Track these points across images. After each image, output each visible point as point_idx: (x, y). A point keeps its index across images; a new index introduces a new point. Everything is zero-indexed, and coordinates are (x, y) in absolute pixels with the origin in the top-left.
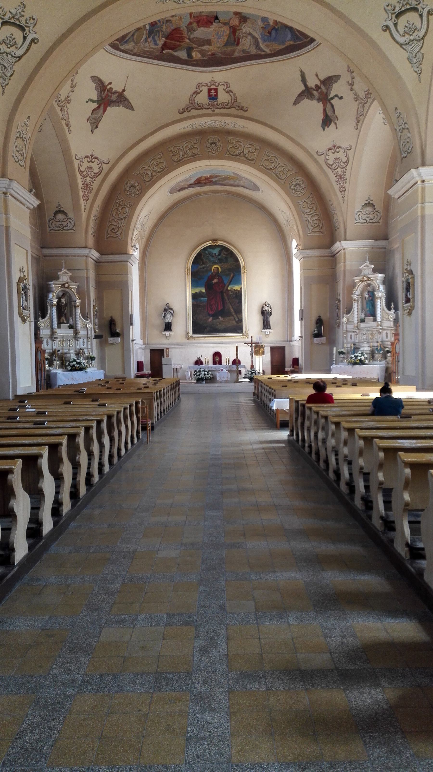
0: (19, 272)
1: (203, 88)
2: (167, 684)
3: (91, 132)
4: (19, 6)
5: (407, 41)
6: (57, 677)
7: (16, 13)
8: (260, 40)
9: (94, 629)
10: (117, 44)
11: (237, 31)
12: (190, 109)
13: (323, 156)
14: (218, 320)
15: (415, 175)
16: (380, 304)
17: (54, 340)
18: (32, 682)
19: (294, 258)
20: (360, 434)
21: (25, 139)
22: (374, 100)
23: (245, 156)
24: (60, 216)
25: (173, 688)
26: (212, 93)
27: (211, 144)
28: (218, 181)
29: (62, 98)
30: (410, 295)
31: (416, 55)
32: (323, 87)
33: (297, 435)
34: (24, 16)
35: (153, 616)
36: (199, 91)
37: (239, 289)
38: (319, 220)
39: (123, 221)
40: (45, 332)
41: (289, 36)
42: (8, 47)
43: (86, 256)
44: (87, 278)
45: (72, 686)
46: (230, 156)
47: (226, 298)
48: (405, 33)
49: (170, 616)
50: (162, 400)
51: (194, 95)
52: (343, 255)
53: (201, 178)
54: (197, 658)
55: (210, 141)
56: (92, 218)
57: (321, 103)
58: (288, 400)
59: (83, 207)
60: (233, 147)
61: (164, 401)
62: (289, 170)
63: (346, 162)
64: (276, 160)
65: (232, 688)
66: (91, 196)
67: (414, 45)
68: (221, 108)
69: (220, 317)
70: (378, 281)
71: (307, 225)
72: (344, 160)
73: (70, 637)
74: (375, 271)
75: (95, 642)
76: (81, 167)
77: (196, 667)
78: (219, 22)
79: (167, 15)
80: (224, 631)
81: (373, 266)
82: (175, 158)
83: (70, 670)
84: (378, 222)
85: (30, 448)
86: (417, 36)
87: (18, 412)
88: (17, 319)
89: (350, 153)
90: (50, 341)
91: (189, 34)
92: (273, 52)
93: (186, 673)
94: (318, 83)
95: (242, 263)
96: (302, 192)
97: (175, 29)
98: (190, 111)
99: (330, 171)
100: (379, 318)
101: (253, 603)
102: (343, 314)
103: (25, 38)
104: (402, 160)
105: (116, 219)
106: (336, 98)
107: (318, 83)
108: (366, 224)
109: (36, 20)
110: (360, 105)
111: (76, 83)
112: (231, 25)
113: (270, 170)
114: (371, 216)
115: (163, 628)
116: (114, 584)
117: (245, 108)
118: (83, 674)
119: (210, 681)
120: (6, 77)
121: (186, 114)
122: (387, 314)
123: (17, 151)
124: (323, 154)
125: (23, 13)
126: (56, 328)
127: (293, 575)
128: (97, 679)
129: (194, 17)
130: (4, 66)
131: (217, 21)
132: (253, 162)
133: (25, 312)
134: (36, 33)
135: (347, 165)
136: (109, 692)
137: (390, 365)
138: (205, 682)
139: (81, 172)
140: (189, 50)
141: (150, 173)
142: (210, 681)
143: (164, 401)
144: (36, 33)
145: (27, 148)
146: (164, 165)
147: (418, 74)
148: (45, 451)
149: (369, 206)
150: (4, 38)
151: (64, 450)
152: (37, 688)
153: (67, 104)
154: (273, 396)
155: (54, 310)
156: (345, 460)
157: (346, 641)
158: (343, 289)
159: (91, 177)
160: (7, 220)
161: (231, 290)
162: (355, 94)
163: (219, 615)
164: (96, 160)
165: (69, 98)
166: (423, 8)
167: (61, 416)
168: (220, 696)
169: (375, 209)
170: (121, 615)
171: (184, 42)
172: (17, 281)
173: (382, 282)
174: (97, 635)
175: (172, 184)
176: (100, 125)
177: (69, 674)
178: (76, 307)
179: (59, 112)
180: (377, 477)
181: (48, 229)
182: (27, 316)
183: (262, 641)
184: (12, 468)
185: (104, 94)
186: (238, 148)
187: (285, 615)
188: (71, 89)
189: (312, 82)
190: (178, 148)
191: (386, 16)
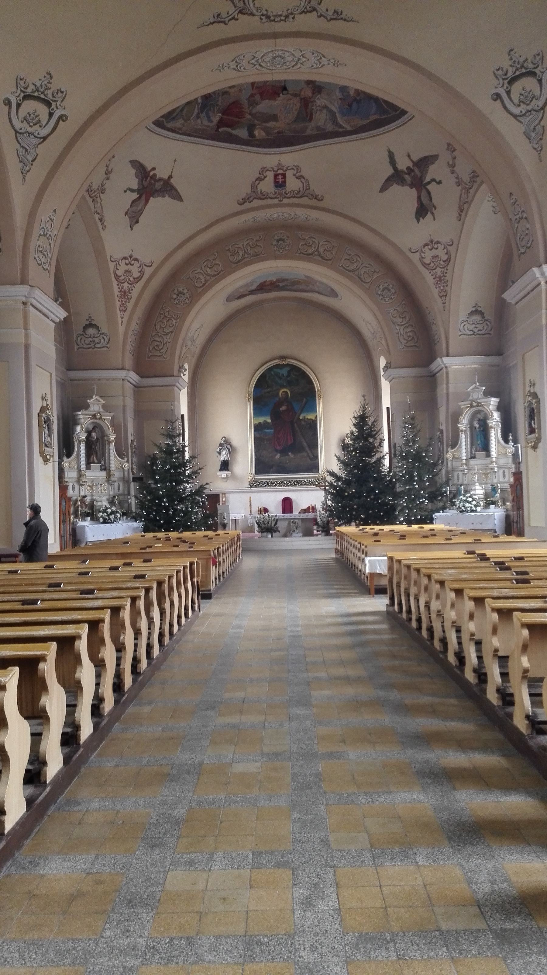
0: (41, 400)
1: (268, 173)
2: (262, 952)
3: (130, 229)
4: (45, 77)
5: (524, 112)
6: (112, 942)
7: (42, 85)
8: (337, 114)
9: (156, 873)
10: (163, 121)
11: (310, 104)
12: (252, 199)
13: (418, 253)
14: (287, 457)
15: (538, 275)
16: (495, 435)
17: (81, 485)
18: (79, 948)
19: (383, 379)
20: (493, 605)
21: (50, 237)
22: (482, 183)
23: (320, 255)
24: (91, 331)
25: (270, 957)
26: (279, 179)
27: (278, 241)
28: (287, 286)
29: (95, 187)
30: (534, 424)
31: (534, 129)
32: (417, 171)
33: (400, 604)
34: (50, 89)
35: (234, 854)
36: (263, 177)
37: (314, 418)
38: (415, 332)
39: (168, 337)
40: (71, 475)
41: (374, 110)
42: (30, 126)
43: (123, 380)
44: (124, 406)
45: (134, 954)
46: (301, 255)
47: (297, 429)
48: (521, 101)
49: (256, 854)
50: (221, 559)
51: (257, 182)
52: (445, 373)
53: (265, 282)
54: (298, 913)
55: (276, 238)
56: (130, 333)
57: (414, 189)
58: (386, 558)
59: (120, 319)
60: (305, 244)
61: (224, 561)
62: (375, 272)
63: (447, 260)
64: (359, 259)
65: (351, 957)
66: (130, 306)
67: (532, 116)
68: (290, 198)
69: (290, 453)
70: (491, 407)
71: (399, 338)
72: (445, 257)
73: (126, 884)
74: (488, 394)
75: (159, 891)
76: (117, 271)
77: (299, 927)
78: (288, 93)
79: (224, 86)
80: (331, 875)
81: (484, 388)
82: (235, 258)
83: (128, 931)
84: (490, 334)
85: (64, 626)
86: (536, 106)
87: (19, 574)
88: (38, 459)
89: (452, 249)
90: (76, 486)
91: (251, 108)
92: (354, 129)
93: (285, 935)
94: (411, 165)
95: (317, 385)
96: (392, 298)
97: (234, 103)
98: (252, 201)
99: (427, 272)
100: (494, 453)
101: (366, 836)
102: (447, 447)
103: (51, 115)
104: (519, 256)
105: (160, 334)
106: (433, 183)
107: (411, 165)
108: (473, 336)
109: (65, 93)
110: (464, 191)
111: (112, 169)
112: (303, 97)
113: (350, 271)
114: (480, 327)
115: (249, 870)
116: (178, 810)
117: (319, 197)
118: (148, 937)
119: (320, 947)
120: (27, 162)
121: (247, 205)
122: (504, 447)
123: (41, 251)
124: (417, 251)
125: (49, 85)
126: (84, 469)
127: (415, 796)
128: (166, 944)
129: (257, 87)
130: (25, 149)
131: (284, 92)
132: (330, 262)
133: (48, 450)
134: (64, 109)
135: (448, 264)
136: (184, 963)
137: (511, 513)
138: (313, 949)
139: (117, 277)
140: (251, 128)
141: (201, 277)
142: (320, 947)
143: (224, 561)
144: (64, 109)
145: (52, 248)
146: (220, 268)
147: (537, 151)
148: (84, 630)
149: (476, 314)
150: (25, 115)
151: (106, 628)
152: (86, 958)
153: (101, 195)
154: (363, 553)
155: (83, 446)
156: (471, 640)
157: (497, 889)
158: (447, 418)
159: (130, 282)
160: (27, 336)
161: (304, 419)
162: (457, 178)
163: (322, 854)
164: (136, 262)
165: (103, 188)
166: (542, 72)
167: (97, 583)
168: (335, 969)
169: (484, 317)
170: (191, 853)
171: (244, 118)
172: (38, 411)
173: (495, 407)
174: (161, 881)
175: (230, 290)
176: (141, 219)
177: (128, 937)
178: (109, 443)
179: (91, 205)
180: (520, 661)
181: (76, 347)
182: (50, 455)
183: (384, 889)
184: (45, 654)
185: (146, 181)
186: (311, 246)
187: (411, 852)
188: (106, 176)
189: (403, 164)
190: (237, 246)
191: (496, 82)
